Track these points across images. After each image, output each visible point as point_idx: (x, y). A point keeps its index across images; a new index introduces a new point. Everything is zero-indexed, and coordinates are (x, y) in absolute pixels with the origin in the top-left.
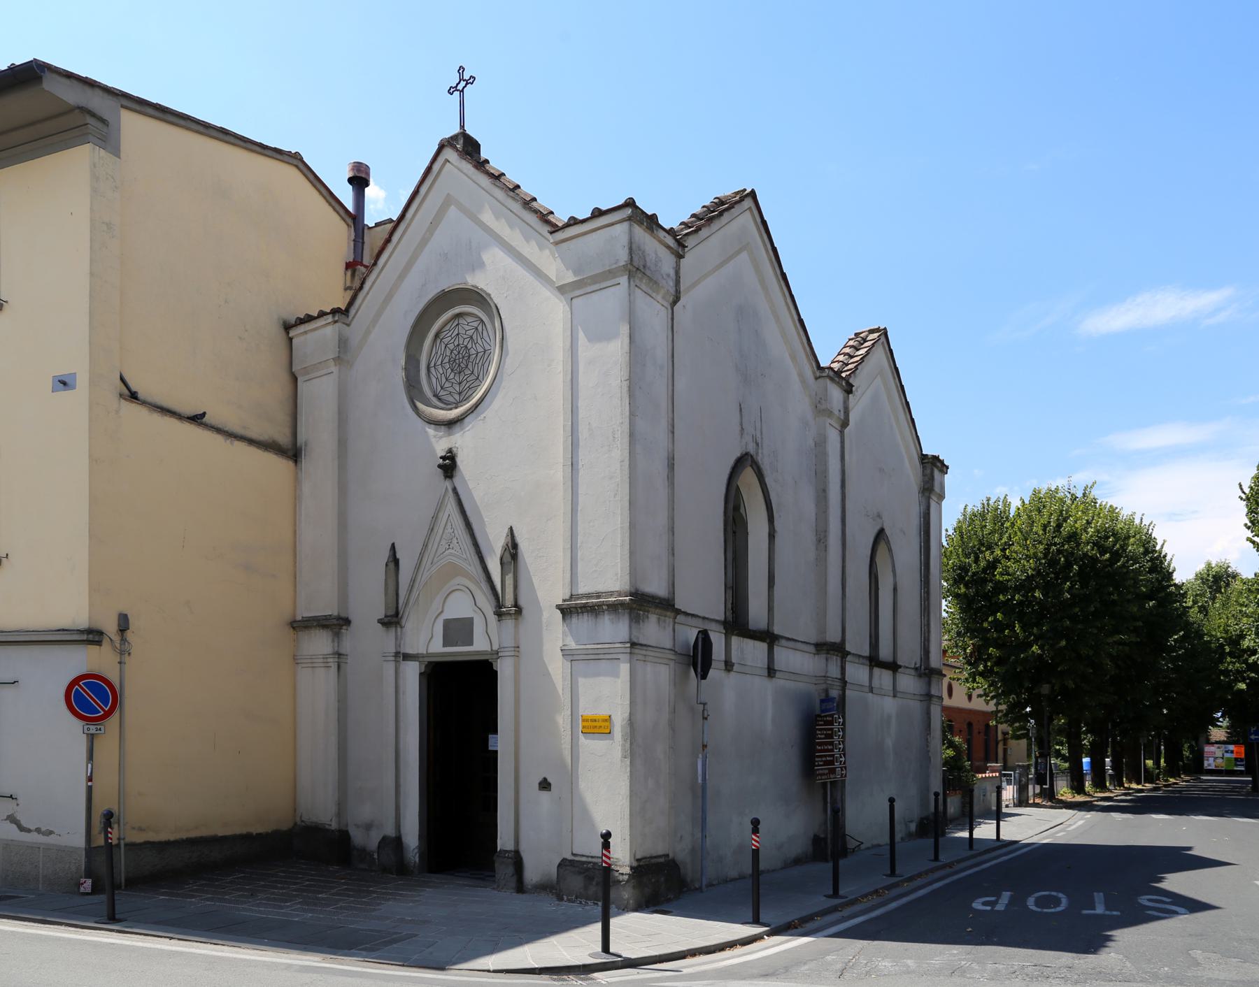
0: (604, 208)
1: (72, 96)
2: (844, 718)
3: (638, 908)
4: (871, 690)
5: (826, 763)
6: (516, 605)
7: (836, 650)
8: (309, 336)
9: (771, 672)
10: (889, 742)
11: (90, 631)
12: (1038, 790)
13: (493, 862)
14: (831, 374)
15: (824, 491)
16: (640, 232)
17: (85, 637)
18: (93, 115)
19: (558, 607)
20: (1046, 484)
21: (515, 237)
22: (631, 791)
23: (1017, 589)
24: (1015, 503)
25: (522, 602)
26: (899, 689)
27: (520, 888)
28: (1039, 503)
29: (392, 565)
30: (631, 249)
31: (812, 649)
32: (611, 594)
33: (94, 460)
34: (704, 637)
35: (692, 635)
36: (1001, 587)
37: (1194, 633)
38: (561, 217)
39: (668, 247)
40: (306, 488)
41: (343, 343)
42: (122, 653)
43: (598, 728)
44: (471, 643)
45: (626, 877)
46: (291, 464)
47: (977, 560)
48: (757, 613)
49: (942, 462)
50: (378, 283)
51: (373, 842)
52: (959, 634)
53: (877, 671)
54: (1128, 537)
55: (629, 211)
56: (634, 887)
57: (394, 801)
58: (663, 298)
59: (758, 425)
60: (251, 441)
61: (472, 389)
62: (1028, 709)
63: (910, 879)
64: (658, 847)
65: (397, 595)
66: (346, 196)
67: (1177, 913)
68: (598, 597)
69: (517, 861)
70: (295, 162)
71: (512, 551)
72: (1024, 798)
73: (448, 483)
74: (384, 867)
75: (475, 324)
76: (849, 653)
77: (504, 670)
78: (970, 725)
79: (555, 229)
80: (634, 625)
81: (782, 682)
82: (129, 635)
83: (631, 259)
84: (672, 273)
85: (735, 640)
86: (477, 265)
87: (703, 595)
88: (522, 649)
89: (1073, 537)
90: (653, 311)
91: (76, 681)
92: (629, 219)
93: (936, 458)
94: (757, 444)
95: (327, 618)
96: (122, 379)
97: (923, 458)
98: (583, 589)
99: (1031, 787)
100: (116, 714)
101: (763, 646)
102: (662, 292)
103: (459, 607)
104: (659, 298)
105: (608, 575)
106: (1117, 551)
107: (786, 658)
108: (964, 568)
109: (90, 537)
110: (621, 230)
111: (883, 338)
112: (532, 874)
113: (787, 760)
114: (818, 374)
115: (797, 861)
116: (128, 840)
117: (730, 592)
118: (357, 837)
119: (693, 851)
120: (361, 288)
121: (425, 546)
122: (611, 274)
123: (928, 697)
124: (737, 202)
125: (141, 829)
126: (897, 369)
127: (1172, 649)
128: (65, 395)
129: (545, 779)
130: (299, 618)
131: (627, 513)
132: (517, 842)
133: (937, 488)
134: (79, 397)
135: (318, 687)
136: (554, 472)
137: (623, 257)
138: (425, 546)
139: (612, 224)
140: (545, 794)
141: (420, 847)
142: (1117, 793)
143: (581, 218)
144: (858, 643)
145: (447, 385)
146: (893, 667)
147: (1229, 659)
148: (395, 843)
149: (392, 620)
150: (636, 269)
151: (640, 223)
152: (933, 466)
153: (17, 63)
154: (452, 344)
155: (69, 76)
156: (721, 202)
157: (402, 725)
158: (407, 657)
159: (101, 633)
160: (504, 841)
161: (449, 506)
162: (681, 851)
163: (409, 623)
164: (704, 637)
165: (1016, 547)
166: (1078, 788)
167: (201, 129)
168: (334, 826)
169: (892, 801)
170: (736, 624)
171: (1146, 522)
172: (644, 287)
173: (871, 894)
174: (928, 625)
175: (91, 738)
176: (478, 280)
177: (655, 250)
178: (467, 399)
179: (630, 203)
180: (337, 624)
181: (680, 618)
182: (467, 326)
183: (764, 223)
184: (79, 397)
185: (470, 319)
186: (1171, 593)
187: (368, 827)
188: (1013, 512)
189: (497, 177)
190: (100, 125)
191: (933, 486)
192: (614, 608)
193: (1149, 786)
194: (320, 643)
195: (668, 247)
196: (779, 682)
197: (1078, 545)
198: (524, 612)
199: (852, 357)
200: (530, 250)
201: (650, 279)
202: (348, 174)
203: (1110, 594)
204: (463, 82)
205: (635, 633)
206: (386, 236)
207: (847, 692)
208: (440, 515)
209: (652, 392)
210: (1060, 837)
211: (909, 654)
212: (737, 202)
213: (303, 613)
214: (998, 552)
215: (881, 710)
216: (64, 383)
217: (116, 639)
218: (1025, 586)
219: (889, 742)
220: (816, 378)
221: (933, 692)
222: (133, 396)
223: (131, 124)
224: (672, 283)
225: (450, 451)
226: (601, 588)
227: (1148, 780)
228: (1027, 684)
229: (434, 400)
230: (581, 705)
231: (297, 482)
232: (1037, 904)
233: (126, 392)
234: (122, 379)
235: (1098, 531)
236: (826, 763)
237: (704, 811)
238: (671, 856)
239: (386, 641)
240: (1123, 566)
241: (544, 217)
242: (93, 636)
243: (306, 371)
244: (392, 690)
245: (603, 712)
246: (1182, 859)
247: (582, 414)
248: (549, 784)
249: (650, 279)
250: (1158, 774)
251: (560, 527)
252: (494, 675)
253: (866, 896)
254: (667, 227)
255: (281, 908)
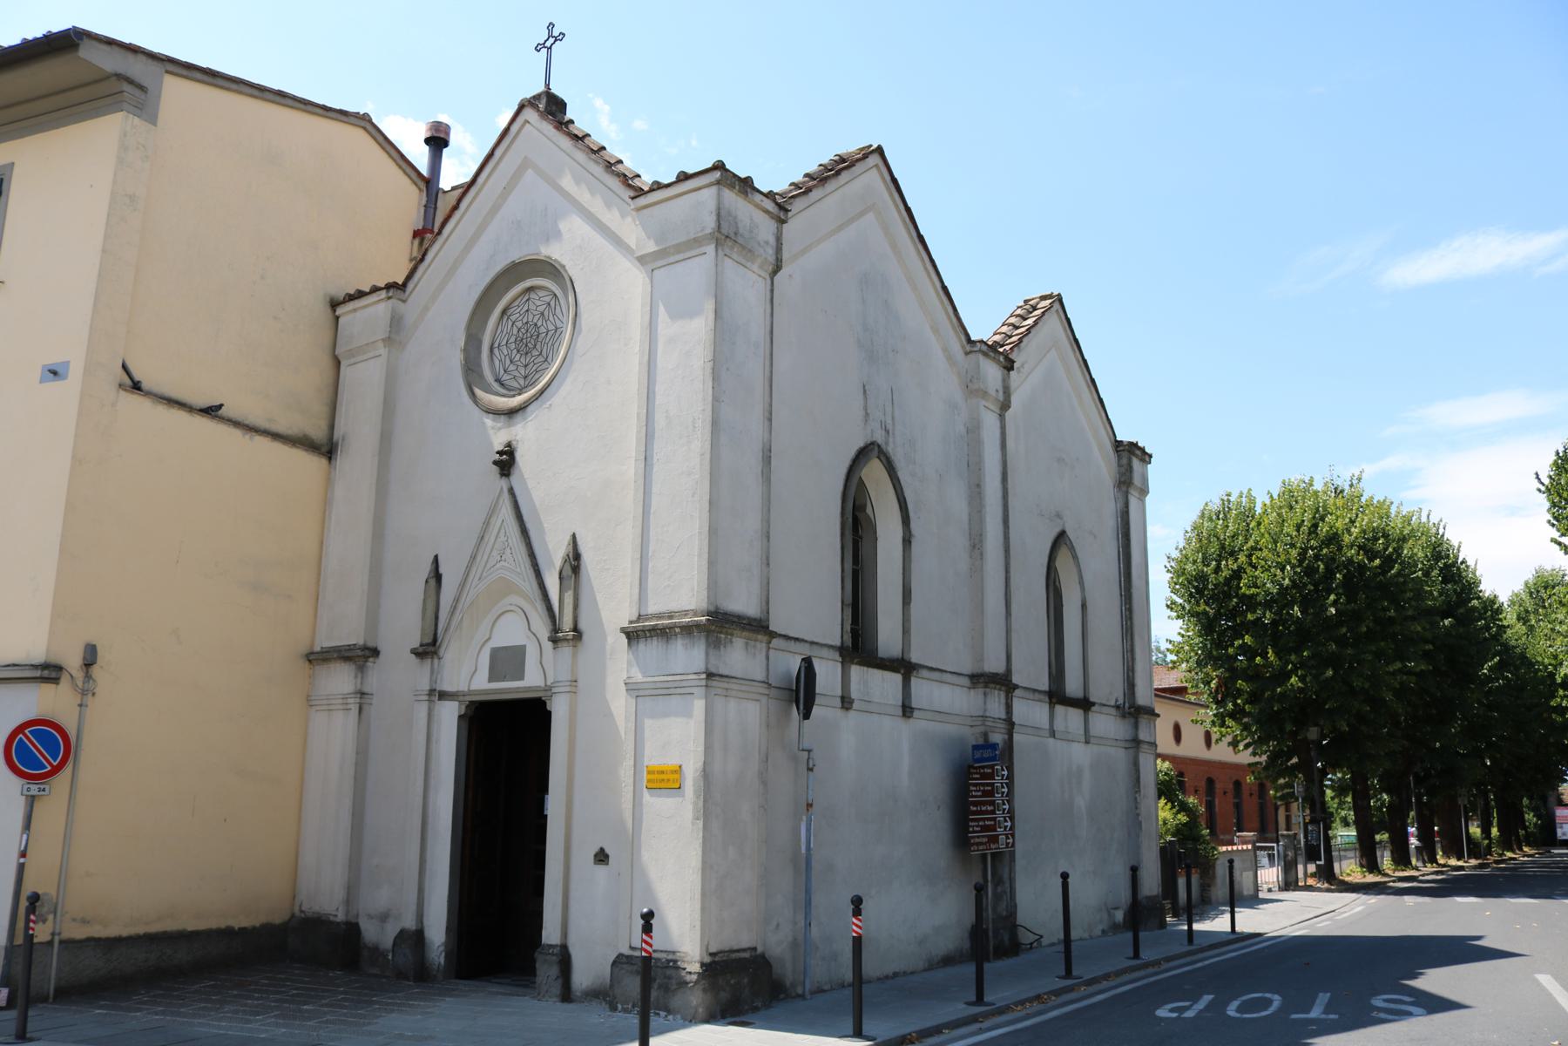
0: (690, 171)
1: (109, 62)
2: (1010, 768)
3: (711, 1018)
4: (1053, 734)
5: (985, 828)
6: (575, 629)
7: (1002, 682)
8: (358, 314)
9: (907, 710)
10: (1081, 802)
11: (45, 666)
12: (1312, 868)
13: (534, 961)
14: (984, 348)
15: (978, 486)
16: (731, 197)
17: (38, 673)
18: (130, 81)
19: (623, 630)
20: (1295, 477)
21: (596, 205)
22: (704, 862)
23: (1268, 605)
24: (1261, 500)
25: (582, 626)
26: (1092, 732)
27: (567, 995)
28: (1290, 497)
29: (433, 582)
30: (718, 215)
31: (966, 681)
32: (686, 613)
33: (77, 460)
34: (808, 663)
35: (795, 664)
36: (1250, 602)
37: (1514, 660)
38: (647, 179)
39: (767, 212)
40: (339, 491)
41: (396, 322)
42: (84, 693)
43: (665, 781)
44: (521, 678)
45: (694, 977)
46: (324, 461)
47: (1217, 570)
48: (888, 639)
49: (1143, 450)
50: (443, 252)
51: (387, 941)
52: (1199, 663)
53: (1059, 709)
54: (1404, 539)
55: (717, 174)
56: (704, 990)
57: (417, 887)
58: (761, 267)
59: (889, 409)
60: (276, 436)
61: (540, 371)
62: (1295, 760)
63: (1090, 982)
64: (741, 938)
65: (437, 618)
66: (420, 156)
67: (1410, 1014)
68: (671, 617)
69: (564, 960)
70: (363, 123)
71: (574, 561)
72: (1292, 879)
73: (503, 483)
74: (403, 970)
75: (547, 299)
76: (1016, 687)
77: (559, 710)
78: (1210, 782)
79: (640, 193)
80: (711, 652)
81: (1095, 748)
82: (95, 670)
83: (719, 227)
84: (772, 240)
85: (856, 671)
86: (553, 234)
87: (812, 610)
88: (580, 684)
89: (1333, 539)
90: (747, 284)
91: (20, 729)
92: (718, 182)
93: (1134, 445)
94: (887, 432)
95: (350, 648)
96: (124, 367)
97: (1118, 445)
98: (652, 608)
99: (1300, 868)
100: (68, 769)
101: (896, 679)
102: (759, 261)
103: (510, 633)
104: (755, 267)
105: (683, 592)
106: (1390, 555)
107: (922, 689)
108: (1201, 577)
109: (61, 551)
110: (709, 195)
111: (1057, 306)
112: (582, 977)
113: (934, 824)
114: (968, 348)
115: (948, 961)
116: (66, 935)
117: (849, 612)
118: (371, 932)
119: (795, 944)
120: (422, 260)
121: (473, 558)
122: (697, 242)
123: (1135, 743)
124: (858, 160)
125: (84, 921)
126: (1076, 341)
127: (1488, 679)
128: (55, 386)
129: (602, 850)
130: (317, 649)
131: (706, 515)
132: (565, 934)
133: (1137, 480)
134: (70, 388)
135: (334, 734)
136: (627, 473)
137: (710, 223)
138: (473, 558)
139: (699, 189)
140: (601, 868)
141: (446, 944)
142: (1425, 872)
143: (666, 182)
144: (1031, 670)
145: (512, 367)
146: (1084, 704)
147: (1561, 692)
148: (415, 939)
149: (428, 650)
150: (726, 236)
151: (732, 187)
152: (1131, 455)
153: (55, 30)
154: (519, 324)
155: (110, 42)
156: (842, 159)
157: (432, 782)
158: (443, 695)
159: (59, 668)
160: (550, 934)
161: (504, 510)
162: (776, 944)
163: (450, 652)
164: (808, 663)
165: (1265, 553)
166: (1372, 865)
167: (256, 93)
168: (341, 917)
169: (1065, 876)
170: (859, 647)
171: (1434, 519)
172: (735, 256)
173: (1030, 1000)
174: (1132, 651)
175: (31, 801)
176: (554, 252)
177: (753, 218)
178: (533, 384)
179: (719, 166)
180: (362, 655)
181: (775, 642)
182: (538, 301)
183: (895, 181)
184: (70, 388)
185: (541, 293)
186: (1474, 609)
187: (384, 918)
188: (1259, 510)
189: (580, 138)
190: (137, 92)
191: (1131, 478)
192: (688, 630)
193: (1473, 862)
194: (340, 679)
195: (767, 212)
196: (918, 724)
197: (1340, 548)
198: (585, 637)
199: (1017, 328)
200: (611, 218)
201: (743, 247)
202: (423, 133)
203: (1385, 609)
204: (553, 38)
205: (712, 660)
206: (453, 202)
207: (1016, 737)
208: (493, 520)
209: (744, 379)
210: (1322, 928)
211: (1107, 686)
212: (858, 160)
213: (324, 642)
214: (1242, 558)
215: (1065, 764)
216: (55, 373)
217: (79, 675)
218: (1281, 600)
219: (1081, 802)
220: (967, 354)
221: (1142, 736)
222: (136, 386)
223: (174, 89)
224: (771, 251)
225: (509, 445)
226: (674, 606)
227: (1472, 855)
228: (1289, 727)
229: (496, 386)
230: (647, 752)
231: (329, 482)
232: (1238, 1010)
233: (128, 382)
234: (124, 367)
235: (1364, 532)
236: (985, 828)
237: (808, 891)
238: (760, 950)
239: (419, 676)
240: (1399, 574)
241: (627, 180)
242: (49, 672)
243: (351, 353)
244: (422, 738)
245: (672, 761)
246: (1462, 950)
247: (659, 400)
248: (607, 856)
249: (743, 247)
250: (1489, 847)
251: (628, 534)
252: (547, 716)
253: (1022, 1003)
254: (765, 190)
255: (249, 1022)
